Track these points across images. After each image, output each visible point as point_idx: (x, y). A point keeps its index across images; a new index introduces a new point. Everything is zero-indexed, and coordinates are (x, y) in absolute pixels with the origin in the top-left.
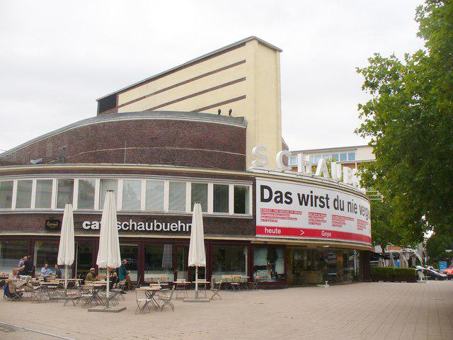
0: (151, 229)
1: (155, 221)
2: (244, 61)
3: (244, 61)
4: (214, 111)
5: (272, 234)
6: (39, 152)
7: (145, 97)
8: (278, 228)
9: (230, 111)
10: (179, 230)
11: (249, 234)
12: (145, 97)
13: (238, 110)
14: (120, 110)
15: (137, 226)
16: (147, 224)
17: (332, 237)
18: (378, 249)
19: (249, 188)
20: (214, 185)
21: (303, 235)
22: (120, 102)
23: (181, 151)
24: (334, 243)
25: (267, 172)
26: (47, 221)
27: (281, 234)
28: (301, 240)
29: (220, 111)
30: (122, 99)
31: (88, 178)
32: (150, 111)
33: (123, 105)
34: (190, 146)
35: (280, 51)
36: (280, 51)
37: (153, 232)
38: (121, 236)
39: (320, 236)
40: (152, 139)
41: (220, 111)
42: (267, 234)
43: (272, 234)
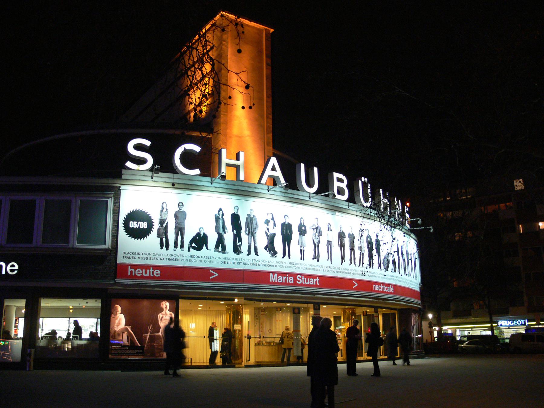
0: (148, 275)
5: (142, 277)
8: (155, 267)
15: (142, 273)
16: (144, 270)
17: (161, 277)
37: (149, 278)
39: (351, 288)
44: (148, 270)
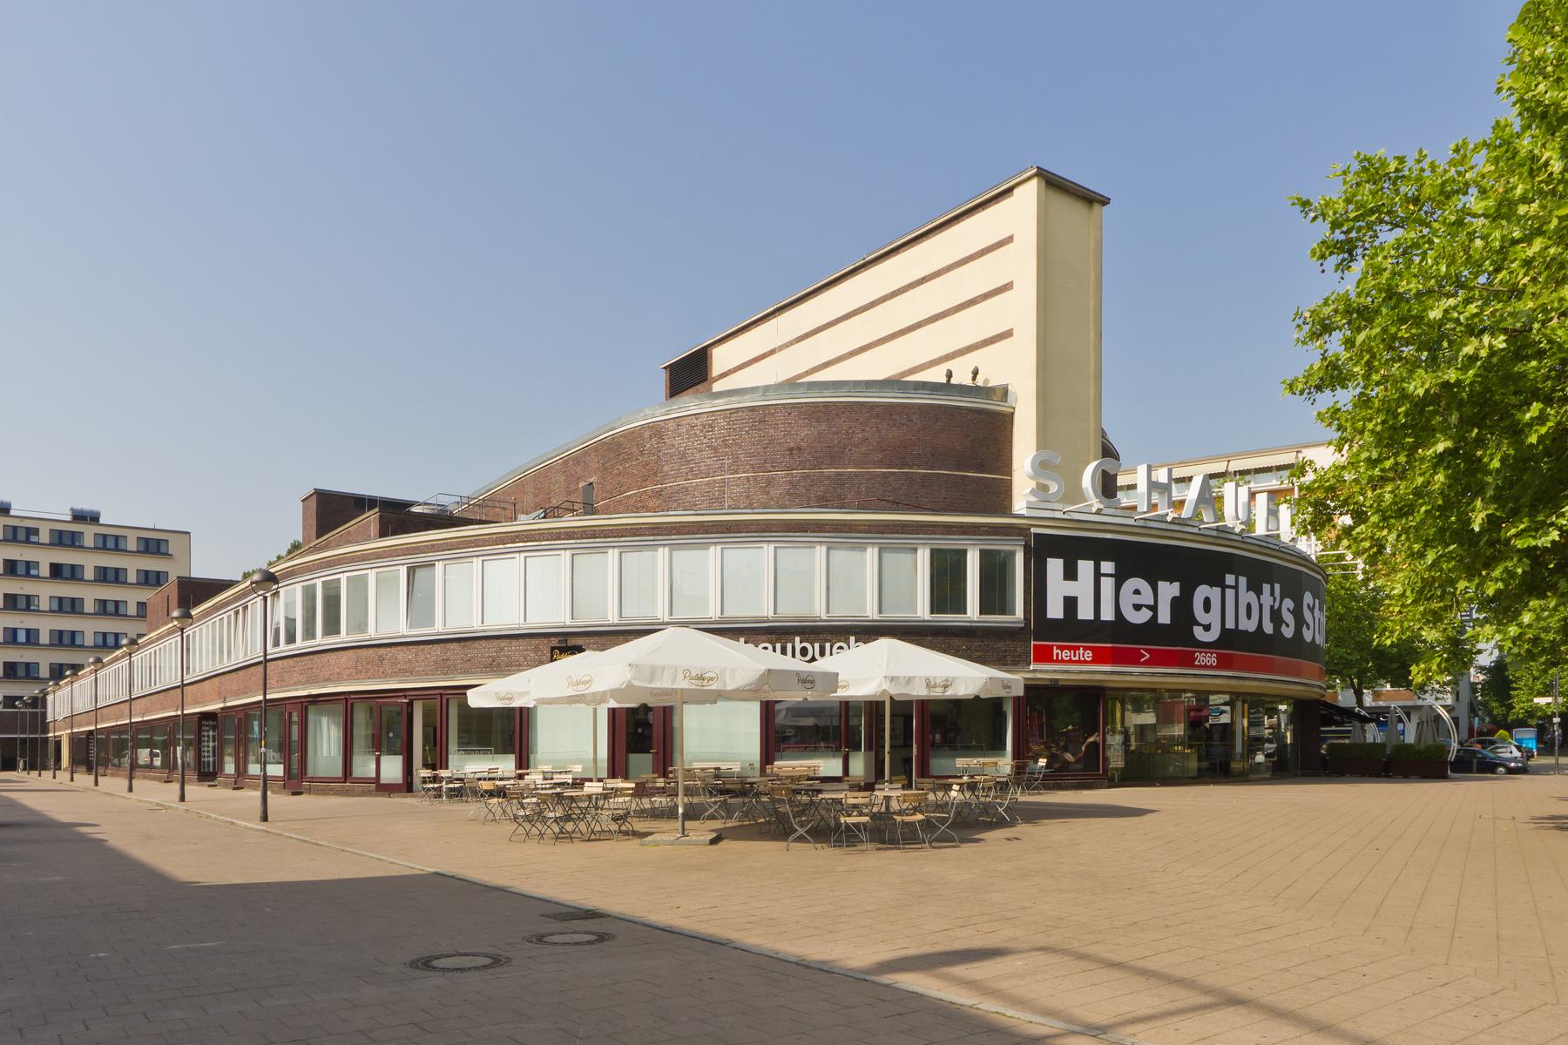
1: (797, 639)
2: (1010, 239)
3: (1010, 239)
4: (936, 375)
6: (536, 495)
7: (772, 352)
9: (975, 373)
10: (1164, 617)
11: (1015, 663)
12: (772, 352)
13: (991, 376)
14: (717, 387)
18: (1345, 698)
19: (1013, 554)
20: (933, 552)
21: (1148, 663)
22: (717, 366)
23: (856, 475)
24: (1225, 681)
25: (1059, 515)
26: (553, 649)
27: (1218, 667)
28: (1142, 674)
29: (949, 375)
30: (721, 359)
31: (329, 575)
32: (791, 384)
33: (1029, 178)
34: (881, 464)
35: (1104, 201)
36: (1104, 201)
38: (1009, 710)
40: (791, 449)
41: (949, 375)
42: (1063, 661)
43: (1070, 661)
44: (789, 646)
